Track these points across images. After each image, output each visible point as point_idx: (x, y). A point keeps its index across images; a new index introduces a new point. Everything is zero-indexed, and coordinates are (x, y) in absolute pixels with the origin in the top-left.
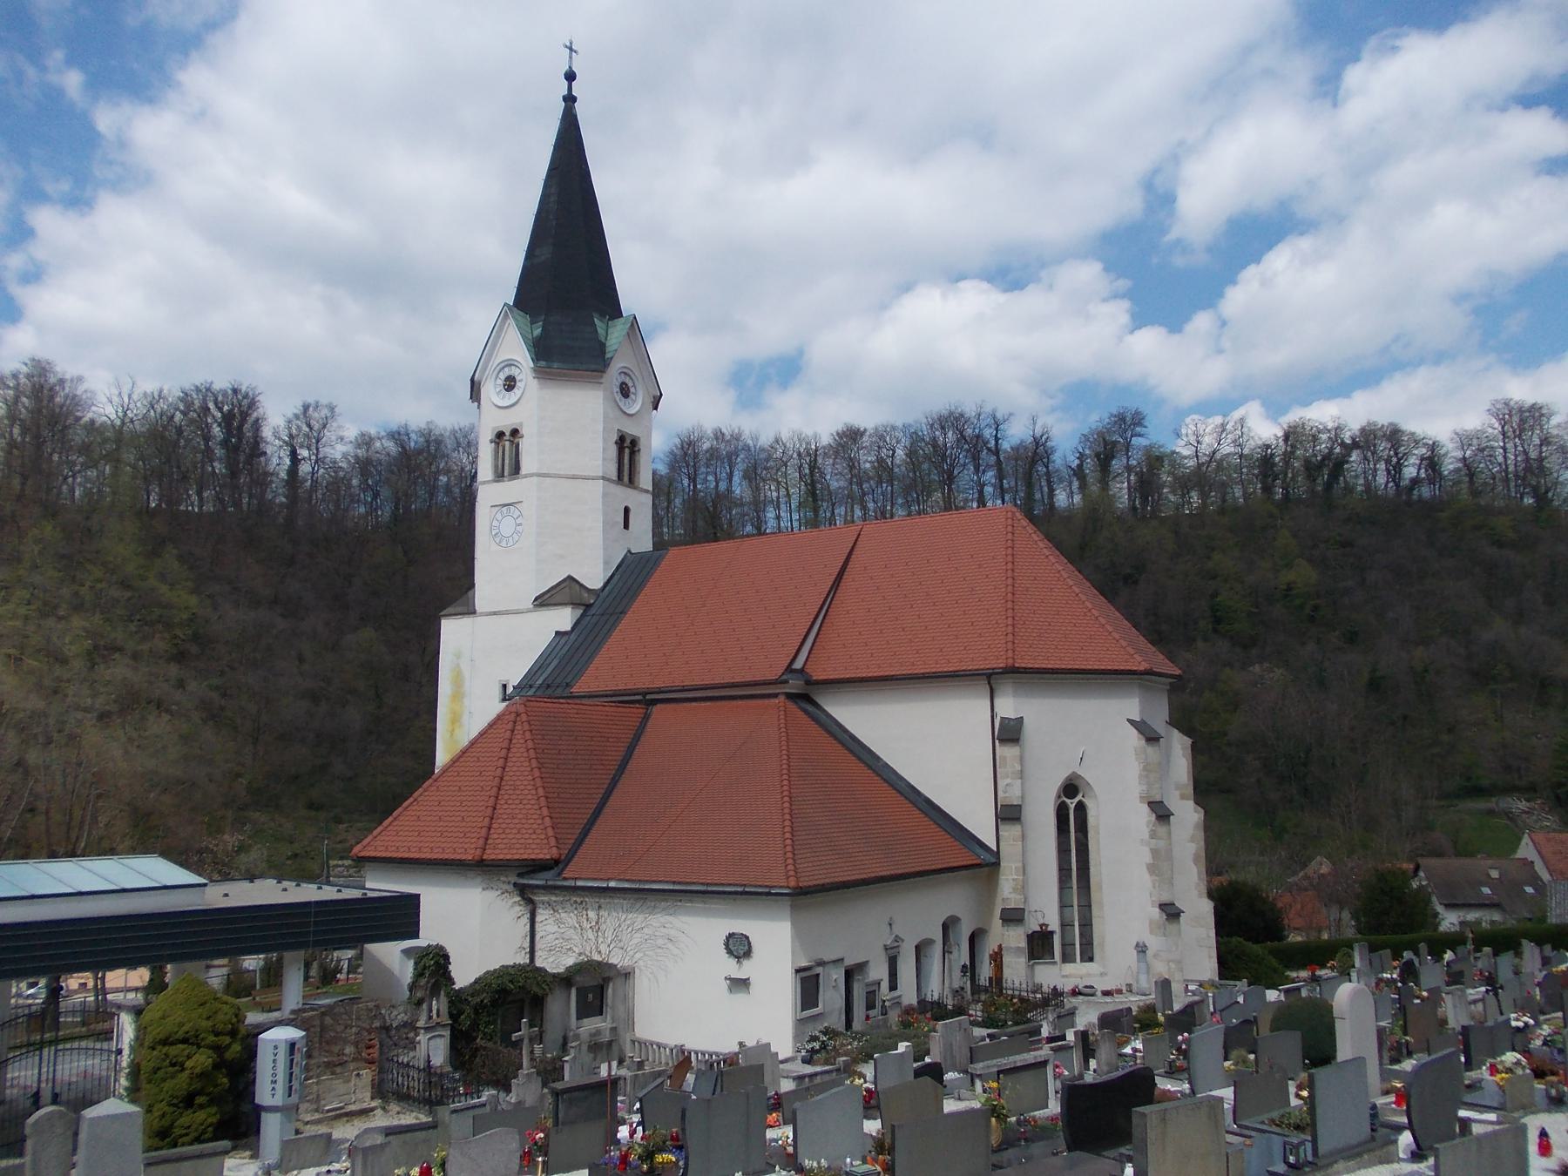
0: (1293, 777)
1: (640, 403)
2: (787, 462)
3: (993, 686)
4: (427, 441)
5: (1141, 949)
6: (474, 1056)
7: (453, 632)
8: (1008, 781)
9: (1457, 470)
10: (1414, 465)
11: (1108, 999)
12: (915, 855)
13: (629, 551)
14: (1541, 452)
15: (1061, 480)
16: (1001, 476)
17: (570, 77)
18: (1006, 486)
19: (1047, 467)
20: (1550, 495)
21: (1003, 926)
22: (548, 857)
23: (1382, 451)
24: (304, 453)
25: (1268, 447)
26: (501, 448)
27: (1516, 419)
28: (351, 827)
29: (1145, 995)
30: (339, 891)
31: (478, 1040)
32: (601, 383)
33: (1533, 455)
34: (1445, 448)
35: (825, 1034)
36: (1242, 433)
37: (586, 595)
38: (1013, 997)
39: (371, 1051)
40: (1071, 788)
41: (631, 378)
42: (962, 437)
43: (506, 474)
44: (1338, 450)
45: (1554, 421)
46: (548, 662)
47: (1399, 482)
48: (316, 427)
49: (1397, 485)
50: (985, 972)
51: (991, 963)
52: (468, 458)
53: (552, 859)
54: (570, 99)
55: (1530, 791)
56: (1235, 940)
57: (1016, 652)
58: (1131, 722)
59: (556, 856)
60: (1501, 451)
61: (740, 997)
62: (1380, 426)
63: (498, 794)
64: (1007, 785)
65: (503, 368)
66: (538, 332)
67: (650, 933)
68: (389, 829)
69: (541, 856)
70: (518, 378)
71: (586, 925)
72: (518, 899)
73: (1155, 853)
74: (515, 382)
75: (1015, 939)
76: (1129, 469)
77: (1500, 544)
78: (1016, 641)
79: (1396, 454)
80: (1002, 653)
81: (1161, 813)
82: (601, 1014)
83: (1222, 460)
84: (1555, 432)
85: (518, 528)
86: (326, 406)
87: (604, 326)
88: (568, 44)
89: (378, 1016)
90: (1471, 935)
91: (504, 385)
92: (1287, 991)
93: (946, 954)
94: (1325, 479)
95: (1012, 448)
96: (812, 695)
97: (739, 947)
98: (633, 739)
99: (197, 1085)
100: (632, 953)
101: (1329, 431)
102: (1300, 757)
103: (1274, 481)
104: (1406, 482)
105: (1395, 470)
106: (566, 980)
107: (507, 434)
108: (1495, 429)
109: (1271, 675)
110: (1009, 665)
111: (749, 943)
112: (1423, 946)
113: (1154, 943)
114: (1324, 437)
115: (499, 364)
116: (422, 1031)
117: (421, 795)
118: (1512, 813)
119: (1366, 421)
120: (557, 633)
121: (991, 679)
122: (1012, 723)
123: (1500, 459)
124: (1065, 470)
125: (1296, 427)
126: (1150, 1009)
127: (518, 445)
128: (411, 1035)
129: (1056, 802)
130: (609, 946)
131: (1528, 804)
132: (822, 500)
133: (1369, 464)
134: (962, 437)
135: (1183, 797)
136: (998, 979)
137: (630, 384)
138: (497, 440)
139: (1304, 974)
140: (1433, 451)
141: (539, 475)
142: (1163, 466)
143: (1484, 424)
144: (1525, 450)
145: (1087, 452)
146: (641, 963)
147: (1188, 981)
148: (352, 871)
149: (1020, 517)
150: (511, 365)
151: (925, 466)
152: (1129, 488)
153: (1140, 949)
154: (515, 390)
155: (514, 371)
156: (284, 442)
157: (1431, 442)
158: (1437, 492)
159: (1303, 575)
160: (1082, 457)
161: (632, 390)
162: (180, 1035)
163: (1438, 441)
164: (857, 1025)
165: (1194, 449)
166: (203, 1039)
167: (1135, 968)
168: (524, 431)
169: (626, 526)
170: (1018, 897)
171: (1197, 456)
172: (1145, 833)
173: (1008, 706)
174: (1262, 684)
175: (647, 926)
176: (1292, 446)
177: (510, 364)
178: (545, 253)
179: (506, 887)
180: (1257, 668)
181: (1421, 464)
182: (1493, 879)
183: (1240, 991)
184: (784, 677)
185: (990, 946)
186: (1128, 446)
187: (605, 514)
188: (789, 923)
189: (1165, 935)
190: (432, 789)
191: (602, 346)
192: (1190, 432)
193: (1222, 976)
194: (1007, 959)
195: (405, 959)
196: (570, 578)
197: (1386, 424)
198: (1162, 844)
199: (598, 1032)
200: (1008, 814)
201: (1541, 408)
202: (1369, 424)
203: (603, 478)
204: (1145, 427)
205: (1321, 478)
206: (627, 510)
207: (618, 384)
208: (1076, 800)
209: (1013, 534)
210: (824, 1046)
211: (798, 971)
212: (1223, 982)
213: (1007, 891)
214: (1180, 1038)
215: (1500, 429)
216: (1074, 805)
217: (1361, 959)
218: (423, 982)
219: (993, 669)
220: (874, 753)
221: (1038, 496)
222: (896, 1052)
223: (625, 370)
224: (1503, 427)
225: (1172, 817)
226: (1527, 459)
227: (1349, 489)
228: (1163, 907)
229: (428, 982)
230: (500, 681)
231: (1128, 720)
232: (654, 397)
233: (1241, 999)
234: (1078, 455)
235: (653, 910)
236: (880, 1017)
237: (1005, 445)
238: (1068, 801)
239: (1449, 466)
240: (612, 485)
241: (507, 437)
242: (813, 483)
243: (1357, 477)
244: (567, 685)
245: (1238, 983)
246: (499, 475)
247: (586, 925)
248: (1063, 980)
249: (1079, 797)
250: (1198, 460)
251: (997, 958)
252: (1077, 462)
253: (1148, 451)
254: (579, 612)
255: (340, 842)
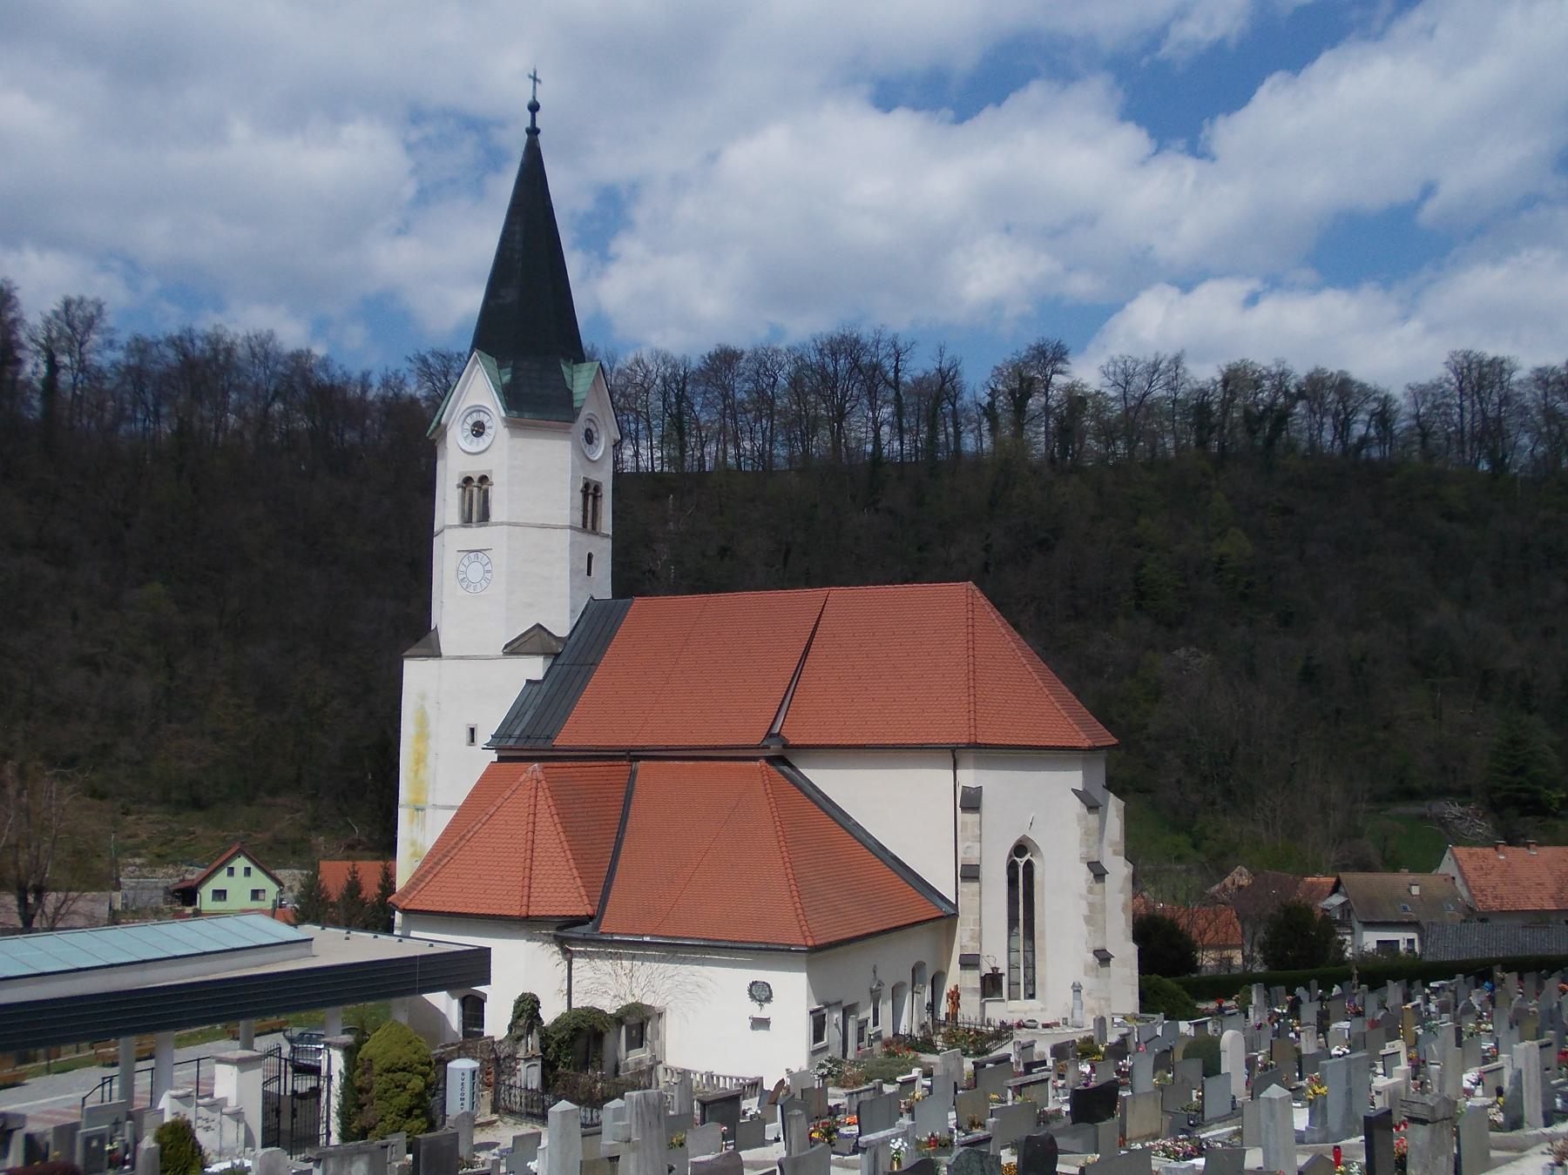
0: (1216, 777)
1: (602, 449)
2: (649, 389)
3: (957, 757)
4: (215, 350)
5: (1077, 989)
6: (555, 1080)
7: (416, 673)
8: (968, 844)
9: (1409, 428)
10: (1363, 421)
11: (1047, 1031)
12: (885, 908)
13: (592, 597)
14: (1500, 412)
15: (970, 421)
16: (899, 413)
17: (534, 108)
18: (905, 425)
19: (954, 405)
20: (1507, 461)
21: (961, 969)
22: (584, 913)
23: (1330, 402)
24: (65, 359)
25: (1205, 393)
26: (467, 493)
27: (1475, 374)
28: (141, 819)
29: (1079, 1027)
30: (431, 945)
31: (560, 1068)
32: (570, 433)
33: (1491, 414)
34: (1397, 404)
35: (830, 1062)
36: (1177, 375)
37: (554, 643)
38: (969, 1030)
39: (489, 1077)
40: (1020, 848)
41: (595, 424)
42: (855, 366)
43: (474, 519)
44: (1281, 400)
45: (1515, 377)
46: (523, 710)
47: (1347, 440)
48: (80, 329)
49: (1344, 443)
50: (944, 1008)
51: (948, 1001)
52: (265, 372)
53: (588, 915)
54: (533, 132)
55: (1464, 794)
56: (1155, 977)
57: (978, 729)
58: (1074, 791)
59: (590, 913)
60: (1458, 410)
61: (761, 1033)
62: (1328, 374)
63: (532, 856)
64: (968, 847)
65: (472, 412)
66: (507, 378)
67: (680, 980)
68: (431, 884)
69: (577, 913)
70: (487, 425)
71: (620, 971)
72: (557, 949)
73: (1091, 905)
74: (484, 430)
75: (972, 979)
76: (1047, 410)
77: (1450, 516)
78: (977, 718)
79: (1345, 408)
80: (965, 729)
81: (1098, 872)
82: (641, 1046)
83: (1153, 405)
84: (1516, 389)
85: (488, 576)
86: (92, 302)
87: (570, 373)
88: (532, 74)
89: (493, 1050)
90: (1356, 972)
91: (472, 431)
92: (1196, 1025)
93: (915, 995)
94: (1267, 434)
95: (914, 382)
96: (787, 757)
97: (761, 993)
98: (626, 797)
99: (415, 1102)
100: (663, 996)
101: (1273, 377)
102: (1224, 755)
103: (1209, 434)
104: (1354, 440)
105: (1343, 427)
106: (619, 1019)
107: (476, 480)
108: (1452, 384)
109: (1198, 661)
110: (973, 741)
111: (770, 991)
112: (1314, 983)
113: (1087, 983)
114: (1267, 383)
115: (465, 411)
116: (523, 1061)
117: (456, 854)
118: (1443, 818)
119: (1314, 368)
120: (528, 681)
121: (954, 754)
122: (972, 792)
123: (1456, 417)
124: (974, 408)
125: (1236, 370)
126: (1089, 1040)
127: (486, 492)
128: (513, 1064)
129: (1008, 860)
130: (642, 990)
131: (1462, 809)
132: (690, 435)
133: (1315, 417)
134: (855, 366)
135: (1115, 853)
136: (952, 1016)
137: (594, 429)
138: (464, 485)
139: (1212, 1005)
140: (1384, 406)
141: (509, 524)
142: (1086, 409)
143: (1441, 378)
144: (1483, 410)
145: (1000, 387)
146: (671, 1004)
147: (1113, 1014)
148: (145, 871)
149: (979, 596)
150: (480, 411)
151: (812, 398)
152: (1046, 432)
153: (1076, 989)
154: (484, 436)
155: (483, 418)
156: (41, 345)
157: (1383, 396)
158: (1387, 454)
159: (1236, 545)
160: (993, 394)
161: (595, 435)
162: (401, 1065)
163: (1391, 395)
164: (851, 1055)
165: (1122, 390)
166: (416, 1068)
167: (1071, 1005)
168: (494, 479)
169: (589, 573)
170: (975, 944)
171: (1125, 399)
172: (1083, 889)
173: (969, 777)
174: (1186, 671)
175: (678, 974)
176: (1232, 392)
177: (479, 409)
178: (510, 295)
179: (546, 938)
180: (1181, 653)
181: (1371, 420)
182: (1413, 896)
183: (1159, 1025)
184: (765, 743)
185: (949, 987)
186: (1048, 383)
187: (572, 563)
188: (805, 974)
189: (1097, 976)
190: (467, 849)
191: (570, 393)
192: (1118, 369)
193: (1142, 1009)
194: (964, 999)
195: (450, 999)
196: (539, 626)
197: (1336, 372)
198: (1097, 899)
199: (640, 1062)
200: (970, 873)
201: (1502, 363)
202: (1317, 371)
203: (571, 528)
204: (1068, 363)
205: (1261, 431)
206: (590, 556)
207: (584, 431)
208: (1025, 859)
209: (973, 612)
210: (830, 1072)
211: (811, 1013)
212: (1143, 1015)
213: (963, 941)
214: (1120, 1063)
215: (1457, 384)
216: (1023, 864)
217: (1258, 997)
218: (522, 1022)
219: (958, 744)
220: (846, 813)
221: (942, 437)
222: (910, 1076)
223: (589, 417)
224: (1461, 383)
225: (1106, 876)
226: (1485, 418)
227: (1291, 447)
228: (1097, 953)
229: (526, 1022)
230: (468, 725)
231: (1073, 790)
232: (615, 440)
233: (1159, 1033)
234: (989, 391)
235: (683, 961)
236: (868, 1048)
237: (906, 378)
238: (1018, 859)
239: (1402, 424)
240: (577, 533)
241: (475, 484)
242: (680, 414)
243: (1300, 431)
244: (548, 737)
245: (1156, 1016)
246: (467, 521)
247: (620, 971)
248: (1011, 1014)
249: (1027, 857)
250: (1126, 403)
251: (955, 997)
252: (988, 399)
253: (1069, 389)
254: (549, 662)
255: (129, 837)
